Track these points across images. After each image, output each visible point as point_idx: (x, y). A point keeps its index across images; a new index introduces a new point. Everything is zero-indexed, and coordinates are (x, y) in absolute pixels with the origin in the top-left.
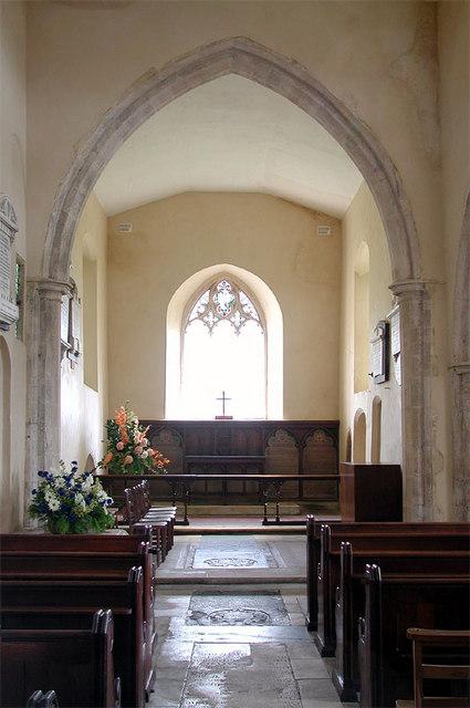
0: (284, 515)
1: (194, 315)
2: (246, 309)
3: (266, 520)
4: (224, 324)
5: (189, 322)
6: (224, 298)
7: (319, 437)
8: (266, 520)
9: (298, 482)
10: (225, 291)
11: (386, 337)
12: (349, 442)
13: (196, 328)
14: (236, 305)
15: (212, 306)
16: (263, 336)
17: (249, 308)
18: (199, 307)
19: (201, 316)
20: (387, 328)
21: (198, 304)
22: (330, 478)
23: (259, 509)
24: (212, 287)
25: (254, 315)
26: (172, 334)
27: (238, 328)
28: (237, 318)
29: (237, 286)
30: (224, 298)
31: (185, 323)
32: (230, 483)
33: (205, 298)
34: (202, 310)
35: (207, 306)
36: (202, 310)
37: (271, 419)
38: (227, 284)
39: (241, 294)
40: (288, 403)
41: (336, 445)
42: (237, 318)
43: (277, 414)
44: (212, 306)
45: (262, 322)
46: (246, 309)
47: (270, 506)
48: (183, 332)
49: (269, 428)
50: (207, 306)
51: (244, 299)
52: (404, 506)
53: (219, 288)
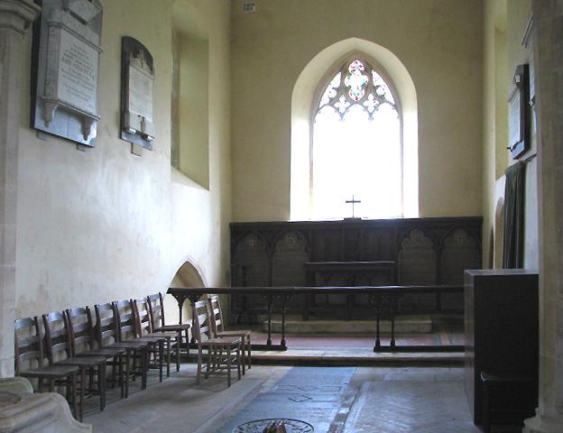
0: (403, 335)
1: (325, 99)
2: (379, 91)
3: (378, 343)
4: (357, 108)
5: (319, 109)
6: (356, 80)
7: (460, 237)
8: (378, 343)
9: (367, 295)
10: (357, 70)
11: (524, 86)
12: (492, 236)
13: (326, 115)
14: (370, 88)
15: (343, 90)
16: (398, 121)
17: (384, 89)
18: (330, 92)
19: (332, 102)
20: (526, 67)
21: (329, 88)
22: (425, 290)
23: (371, 325)
24: (342, 67)
25: (389, 97)
26: (299, 125)
27: (371, 114)
28: (371, 102)
29: (370, 66)
30: (356, 80)
31: (314, 109)
32: (317, 296)
33: (336, 82)
34: (334, 94)
35: (337, 90)
36: (334, 94)
37: (407, 216)
38: (359, 64)
39: (375, 74)
40: (426, 191)
41: (479, 249)
42: (371, 102)
43: (412, 211)
44: (343, 90)
45: (398, 106)
46: (379, 91)
47: (385, 326)
48: (312, 120)
49: (404, 226)
50: (337, 90)
51: (377, 79)
52: (541, 354)
53: (350, 69)
